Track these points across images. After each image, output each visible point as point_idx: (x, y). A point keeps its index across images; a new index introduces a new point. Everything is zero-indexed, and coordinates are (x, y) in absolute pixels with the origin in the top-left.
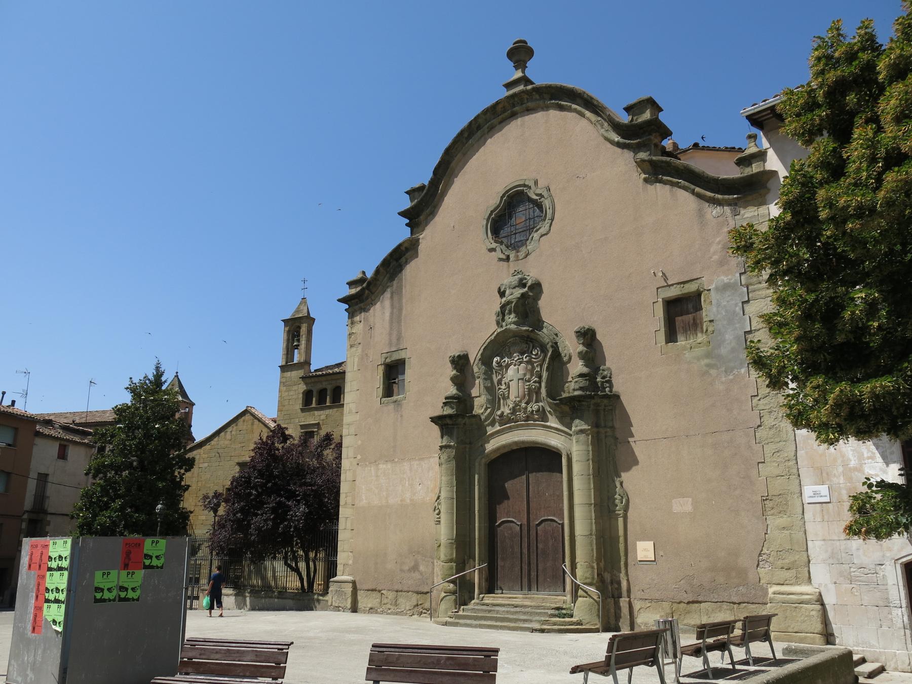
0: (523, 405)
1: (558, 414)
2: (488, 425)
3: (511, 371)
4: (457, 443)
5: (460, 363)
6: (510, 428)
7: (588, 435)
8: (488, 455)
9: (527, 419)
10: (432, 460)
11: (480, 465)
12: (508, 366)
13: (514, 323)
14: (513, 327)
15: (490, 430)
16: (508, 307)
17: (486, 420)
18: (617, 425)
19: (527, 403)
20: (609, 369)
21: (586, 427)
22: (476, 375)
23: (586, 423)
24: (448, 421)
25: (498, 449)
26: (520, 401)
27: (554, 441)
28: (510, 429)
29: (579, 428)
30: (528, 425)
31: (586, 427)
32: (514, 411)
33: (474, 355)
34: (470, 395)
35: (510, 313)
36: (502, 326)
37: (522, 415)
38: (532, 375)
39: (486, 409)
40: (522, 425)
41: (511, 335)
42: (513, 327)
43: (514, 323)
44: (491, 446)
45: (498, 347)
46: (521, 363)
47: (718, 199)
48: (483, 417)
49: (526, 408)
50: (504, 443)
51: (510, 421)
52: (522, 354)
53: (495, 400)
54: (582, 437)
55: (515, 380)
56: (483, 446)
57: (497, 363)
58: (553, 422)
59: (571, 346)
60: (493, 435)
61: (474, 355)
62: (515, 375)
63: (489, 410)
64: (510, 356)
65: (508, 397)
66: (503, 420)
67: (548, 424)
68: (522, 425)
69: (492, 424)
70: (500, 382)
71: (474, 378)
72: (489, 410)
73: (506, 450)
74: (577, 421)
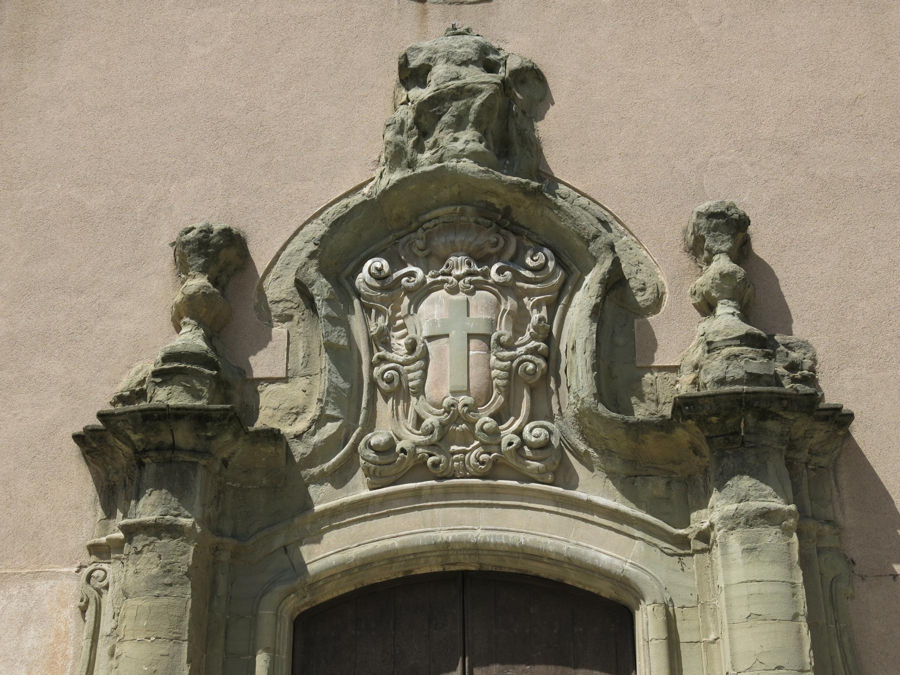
0: (485, 420)
1: (617, 466)
2: (319, 480)
3: (435, 310)
4: (205, 521)
5: (219, 256)
6: (417, 495)
7: (787, 532)
8: (315, 584)
9: (494, 469)
10: (41, 586)
11: (277, 617)
12: (420, 293)
13: (475, 156)
14: (468, 166)
15: (324, 498)
16: (455, 107)
17: (311, 460)
18: (848, 518)
19: (499, 417)
20: (804, 345)
21: (777, 504)
22: (277, 309)
23: (780, 492)
24: (183, 435)
25: (348, 570)
26: (472, 408)
27: (609, 551)
28: (416, 500)
29: (755, 505)
30: (495, 492)
31: (777, 504)
32: (443, 437)
33: (279, 248)
34: (244, 371)
35: (459, 124)
36: (411, 165)
37: (475, 454)
38: (518, 331)
39: (319, 422)
40: (468, 492)
41: (446, 194)
42: (468, 166)
43: (475, 156)
44: (324, 555)
45: (380, 237)
46: (478, 286)
47: (176, 361)
48: (299, 450)
49: (495, 434)
50: (396, 543)
51: (417, 468)
52: (484, 260)
53: (352, 399)
54: (770, 536)
55: (457, 335)
56: (290, 550)
57: (379, 275)
58: (595, 487)
59: (658, 260)
60: (337, 516)
61: (279, 248)
62: (449, 328)
63: (330, 428)
64: (432, 259)
65: (420, 391)
66: (390, 464)
67: (578, 493)
68: (468, 492)
69: (340, 477)
70: (382, 340)
71: (265, 317)
72: (330, 428)
73: (395, 572)
74: (745, 483)
